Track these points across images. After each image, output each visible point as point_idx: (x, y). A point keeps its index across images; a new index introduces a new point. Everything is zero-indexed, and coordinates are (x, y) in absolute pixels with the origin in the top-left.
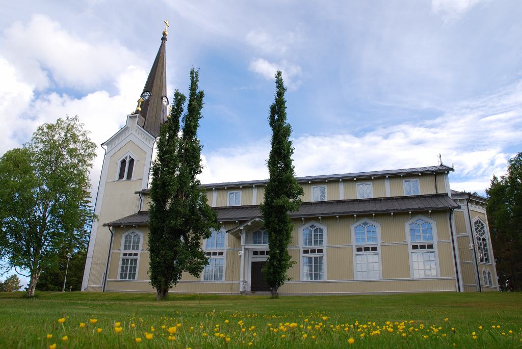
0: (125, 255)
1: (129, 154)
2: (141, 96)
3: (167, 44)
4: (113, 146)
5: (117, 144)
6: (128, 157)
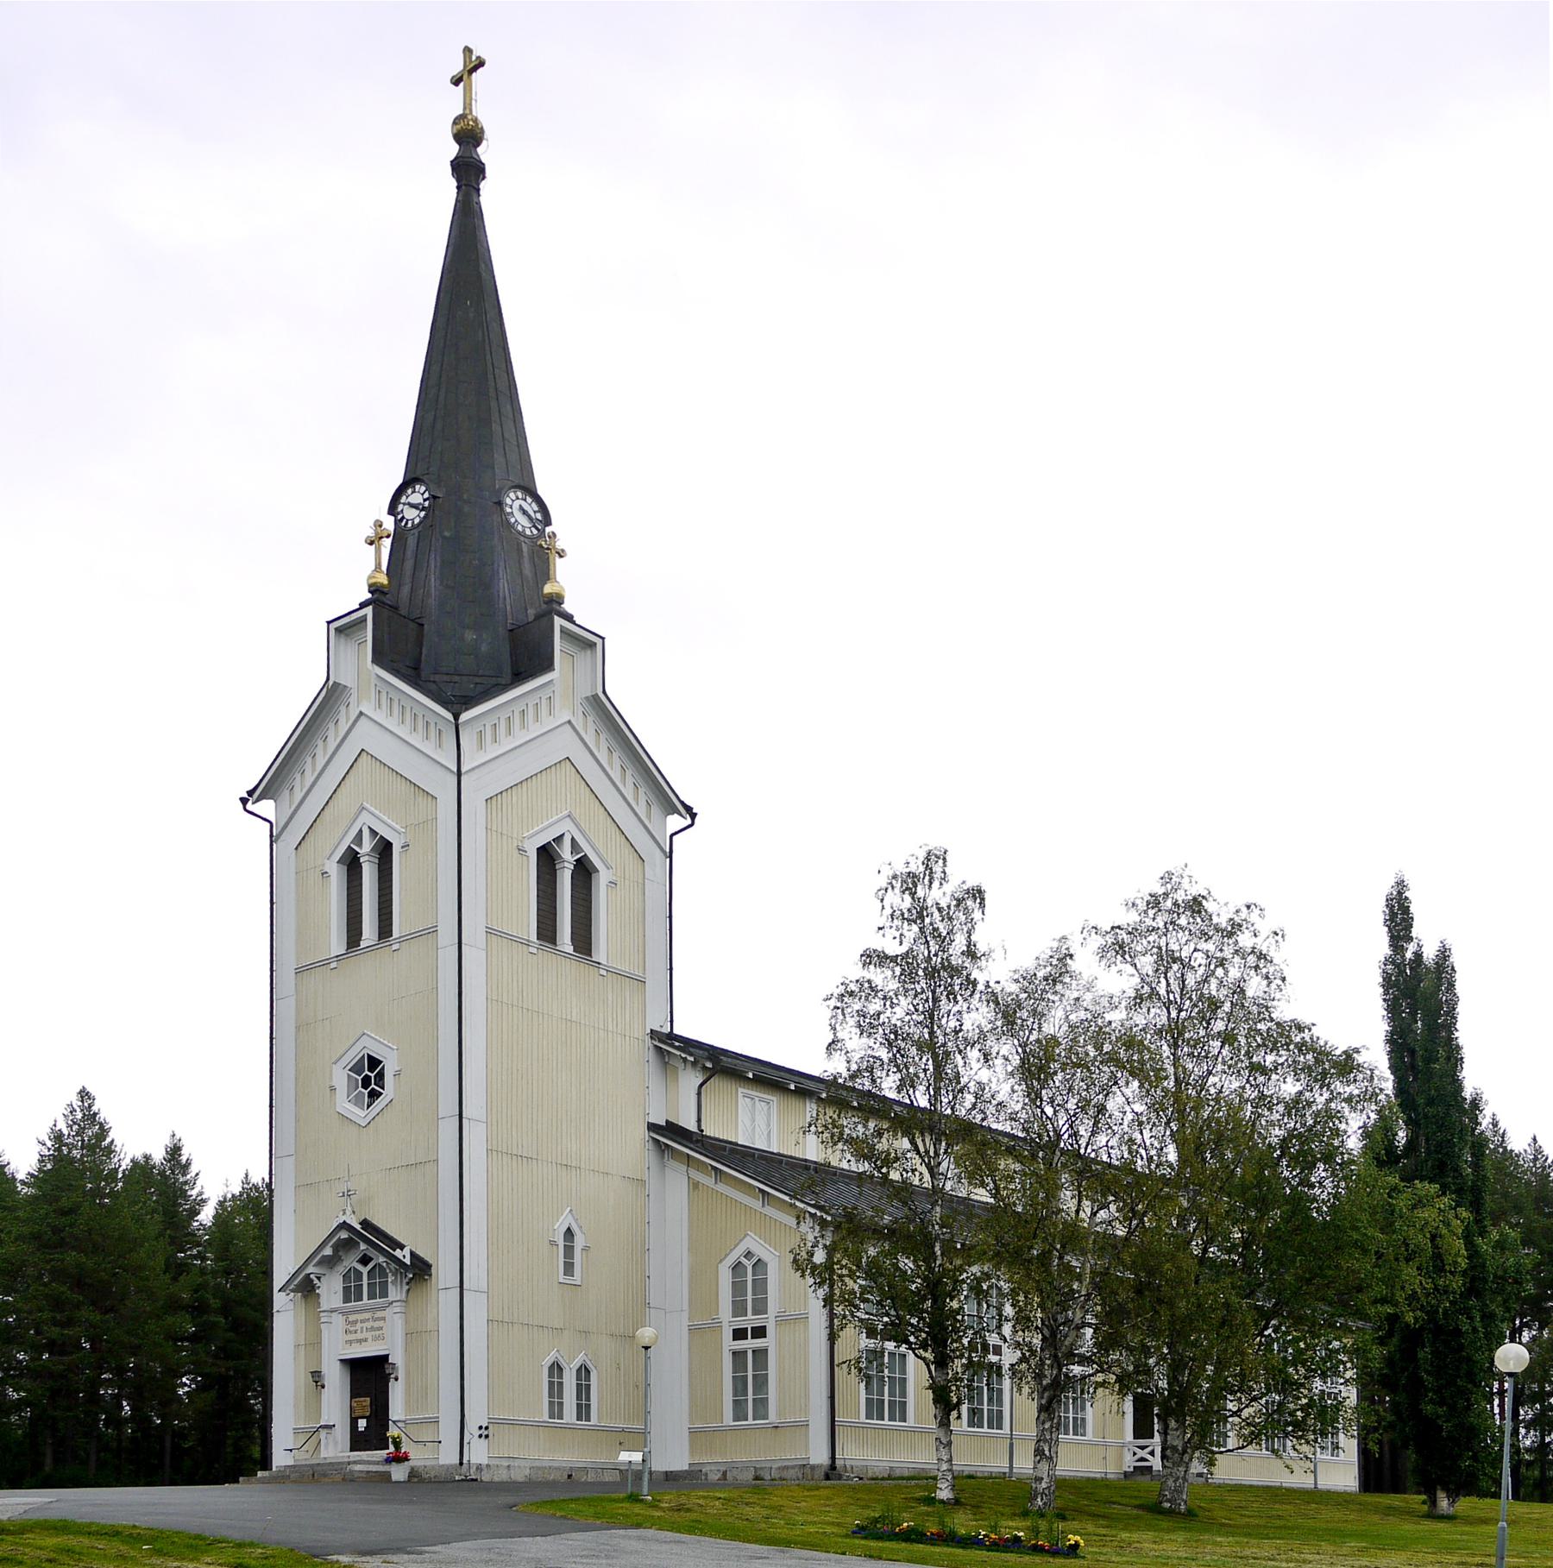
0: (739, 1334)
1: (365, 820)
2: (392, 510)
3: (490, 195)
4: (298, 795)
5: (309, 779)
6: (366, 833)
